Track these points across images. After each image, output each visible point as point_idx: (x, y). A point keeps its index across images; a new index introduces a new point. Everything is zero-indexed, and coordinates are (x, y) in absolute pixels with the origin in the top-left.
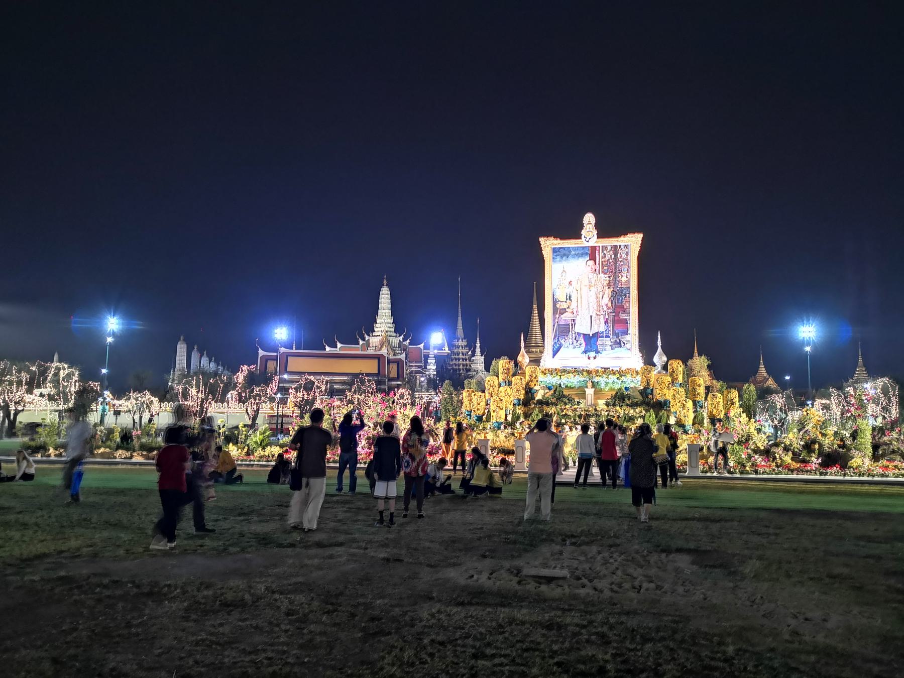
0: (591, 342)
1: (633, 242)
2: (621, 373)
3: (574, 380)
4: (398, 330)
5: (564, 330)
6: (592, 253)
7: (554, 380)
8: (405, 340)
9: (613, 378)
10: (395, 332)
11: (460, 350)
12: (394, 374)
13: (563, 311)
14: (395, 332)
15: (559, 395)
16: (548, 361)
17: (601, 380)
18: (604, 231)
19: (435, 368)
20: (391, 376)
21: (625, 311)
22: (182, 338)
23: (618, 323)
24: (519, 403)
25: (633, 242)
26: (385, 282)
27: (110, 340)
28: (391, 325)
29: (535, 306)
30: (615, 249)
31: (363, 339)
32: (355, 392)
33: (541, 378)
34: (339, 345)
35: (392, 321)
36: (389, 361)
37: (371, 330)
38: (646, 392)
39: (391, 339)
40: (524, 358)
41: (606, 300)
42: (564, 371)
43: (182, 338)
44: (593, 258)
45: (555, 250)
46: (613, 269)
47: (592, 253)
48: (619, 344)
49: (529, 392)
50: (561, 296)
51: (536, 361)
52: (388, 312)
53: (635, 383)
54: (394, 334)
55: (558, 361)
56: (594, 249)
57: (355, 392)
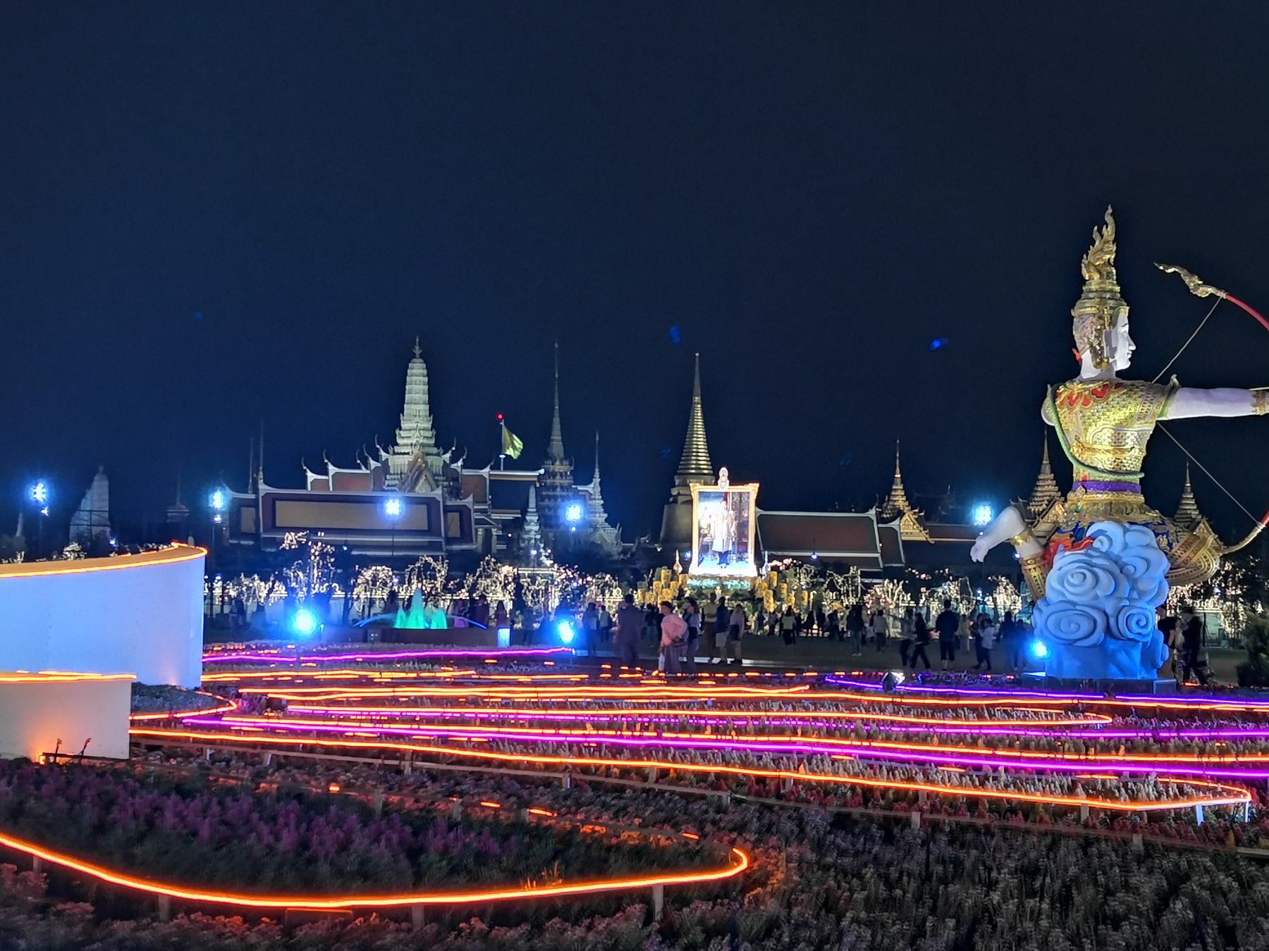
0: (723, 557)
1: (752, 489)
2: (741, 579)
3: (711, 583)
4: (441, 442)
5: (705, 549)
6: (725, 496)
7: (695, 583)
8: (454, 459)
9: (735, 582)
10: (436, 445)
11: (558, 481)
12: (455, 531)
13: (705, 535)
14: (436, 445)
15: (700, 592)
16: (694, 569)
17: (729, 584)
18: (734, 480)
19: (537, 528)
20: (451, 534)
21: (747, 537)
22: (101, 468)
23: (741, 546)
24: (675, 598)
25: (752, 489)
26: (417, 351)
27: (574, 529)
28: (429, 434)
29: (697, 399)
30: (741, 494)
31: (377, 458)
32: (480, 576)
33: (689, 582)
34: (332, 469)
35: (429, 425)
36: (447, 510)
37: (390, 442)
38: (753, 592)
39: (430, 459)
40: (678, 568)
41: (733, 529)
42: (705, 577)
43: (101, 468)
44: (726, 499)
45: (700, 493)
46: (739, 507)
47: (725, 496)
48: (740, 559)
49: (682, 592)
50: (704, 525)
51: (685, 571)
52: (424, 409)
53: (747, 585)
54: (435, 450)
55: (703, 570)
56: (726, 493)
57: (480, 576)
